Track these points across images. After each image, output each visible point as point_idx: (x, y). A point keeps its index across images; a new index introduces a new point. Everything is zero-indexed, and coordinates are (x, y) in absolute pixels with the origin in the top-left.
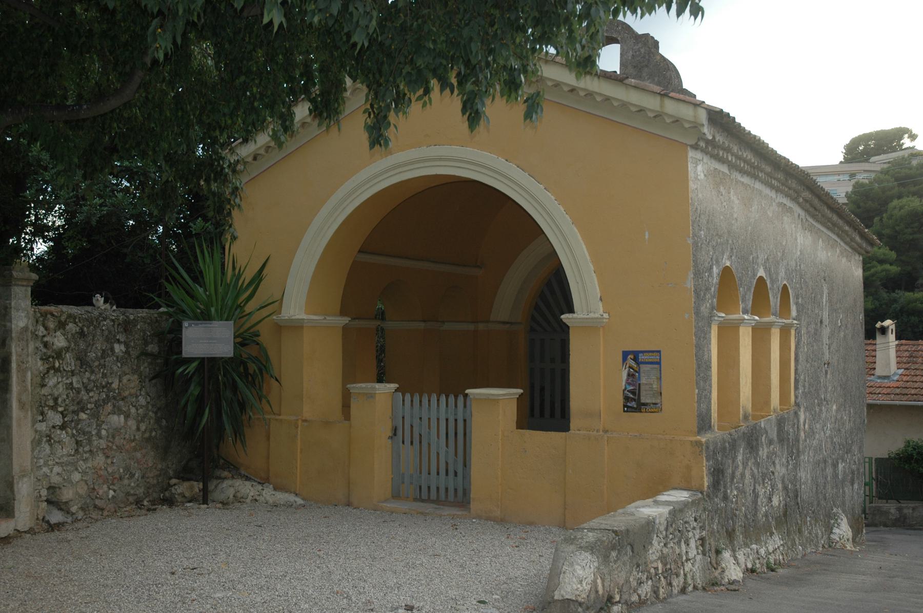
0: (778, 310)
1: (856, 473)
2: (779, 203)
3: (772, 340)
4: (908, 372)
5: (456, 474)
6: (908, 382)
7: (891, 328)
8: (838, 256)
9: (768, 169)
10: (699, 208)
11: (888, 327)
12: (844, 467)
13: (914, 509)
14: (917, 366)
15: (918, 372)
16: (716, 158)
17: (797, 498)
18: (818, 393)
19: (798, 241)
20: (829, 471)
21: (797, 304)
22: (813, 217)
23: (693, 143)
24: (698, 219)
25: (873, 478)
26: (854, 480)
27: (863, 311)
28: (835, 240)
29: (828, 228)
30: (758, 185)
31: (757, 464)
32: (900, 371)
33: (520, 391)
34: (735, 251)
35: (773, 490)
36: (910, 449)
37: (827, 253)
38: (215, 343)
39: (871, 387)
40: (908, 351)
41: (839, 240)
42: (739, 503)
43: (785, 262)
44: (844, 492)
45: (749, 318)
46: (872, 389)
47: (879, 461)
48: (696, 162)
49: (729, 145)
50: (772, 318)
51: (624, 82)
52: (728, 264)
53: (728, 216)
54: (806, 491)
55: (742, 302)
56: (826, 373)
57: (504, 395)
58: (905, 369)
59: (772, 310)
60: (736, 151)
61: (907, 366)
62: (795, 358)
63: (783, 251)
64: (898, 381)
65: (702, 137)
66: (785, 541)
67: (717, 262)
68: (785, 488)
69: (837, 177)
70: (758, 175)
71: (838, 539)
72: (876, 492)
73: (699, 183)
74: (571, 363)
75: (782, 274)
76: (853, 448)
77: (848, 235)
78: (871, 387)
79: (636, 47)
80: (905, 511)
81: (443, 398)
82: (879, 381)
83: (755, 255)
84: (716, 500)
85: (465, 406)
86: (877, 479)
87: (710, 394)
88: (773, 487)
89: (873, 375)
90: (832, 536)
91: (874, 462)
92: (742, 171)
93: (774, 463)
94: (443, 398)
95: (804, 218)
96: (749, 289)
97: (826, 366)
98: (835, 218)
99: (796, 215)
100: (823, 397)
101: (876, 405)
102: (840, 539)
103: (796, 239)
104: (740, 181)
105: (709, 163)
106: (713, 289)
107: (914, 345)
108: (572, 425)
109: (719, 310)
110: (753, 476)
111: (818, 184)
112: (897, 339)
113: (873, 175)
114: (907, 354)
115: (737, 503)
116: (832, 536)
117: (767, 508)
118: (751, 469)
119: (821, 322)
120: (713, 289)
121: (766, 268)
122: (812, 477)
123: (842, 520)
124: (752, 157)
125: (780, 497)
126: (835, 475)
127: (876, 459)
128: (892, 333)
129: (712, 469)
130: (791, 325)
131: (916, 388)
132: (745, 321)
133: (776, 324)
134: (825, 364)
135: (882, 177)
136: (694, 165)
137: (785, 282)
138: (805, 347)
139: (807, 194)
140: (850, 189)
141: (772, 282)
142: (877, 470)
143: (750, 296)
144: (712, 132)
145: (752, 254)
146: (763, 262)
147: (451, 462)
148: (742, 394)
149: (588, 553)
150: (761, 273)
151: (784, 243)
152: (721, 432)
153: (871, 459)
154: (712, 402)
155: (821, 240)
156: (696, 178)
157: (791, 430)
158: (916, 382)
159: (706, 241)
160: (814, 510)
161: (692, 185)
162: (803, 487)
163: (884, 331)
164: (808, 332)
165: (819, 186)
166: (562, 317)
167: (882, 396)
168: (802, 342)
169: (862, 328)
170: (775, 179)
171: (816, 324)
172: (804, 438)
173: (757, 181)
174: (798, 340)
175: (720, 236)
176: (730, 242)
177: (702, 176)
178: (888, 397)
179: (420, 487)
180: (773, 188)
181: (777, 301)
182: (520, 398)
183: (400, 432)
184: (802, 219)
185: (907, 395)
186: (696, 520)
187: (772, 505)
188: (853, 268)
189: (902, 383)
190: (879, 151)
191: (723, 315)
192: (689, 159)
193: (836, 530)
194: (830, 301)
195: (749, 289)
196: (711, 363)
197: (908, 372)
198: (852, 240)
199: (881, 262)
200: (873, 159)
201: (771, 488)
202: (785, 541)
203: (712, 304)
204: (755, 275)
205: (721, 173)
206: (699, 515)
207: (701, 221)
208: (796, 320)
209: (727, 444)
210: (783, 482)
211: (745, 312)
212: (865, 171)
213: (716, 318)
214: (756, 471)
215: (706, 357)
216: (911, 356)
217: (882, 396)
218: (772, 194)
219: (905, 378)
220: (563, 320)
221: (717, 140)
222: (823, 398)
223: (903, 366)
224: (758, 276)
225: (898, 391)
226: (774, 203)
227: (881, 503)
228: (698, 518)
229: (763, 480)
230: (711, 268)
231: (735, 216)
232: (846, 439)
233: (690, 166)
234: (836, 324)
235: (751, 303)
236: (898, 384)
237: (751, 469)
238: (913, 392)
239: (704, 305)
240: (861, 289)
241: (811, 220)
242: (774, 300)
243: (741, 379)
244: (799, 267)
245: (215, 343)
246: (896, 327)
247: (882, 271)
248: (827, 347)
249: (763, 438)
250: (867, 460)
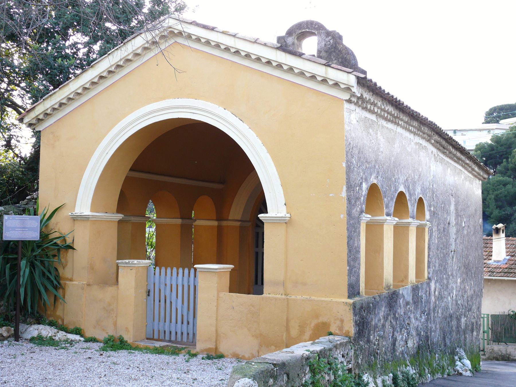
0: (415, 213)
1: (475, 324)
2: (416, 143)
3: (410, 234)
5: (188, 323)
7: (502, 229)
8: (463, 180)
9: (406, 119)
10: (352, 143)
12: (466, 321)
16: (365, 109)
17: (428, 341)
18: (446, 271)
19: (432, 169)
21: (430, 210)
22: (444, 153)
23: (347, 98)
24: (351, 150)
25: (489, 328)
26: (473, 329)
28: (460, 170)
29: (455, 161)
30: (399, 130)
31: (396, 319)
33: (232, 266)
34: (381, 173)
35: (408, 336)
37: (454, 178)
38: (27, 231)
41: (463, 170)
42: (380, 345)
43: (421, 183)
44: (465, 338)
45: (390, 219)
47: (493, 316)
48: (350, 111)
49: (374, 101)
50: (410, 220)
51: (302, 57)
52: (375, 182)
53: (376, 149)
54: (436, 337)
55: (386, 208)
56: (453, 257)
57: (220, 269)
59: (410, 214)
60: (379, 106)
62: (428, 247)
63: (420, 175)
65: (353, 95)
66: (417, 371)
67: (366, 180)
68: (419, 334)
70: (398, 123)
72: (492, 337)
73: (353, 126)
75: (418, 190)
77: (470, 167)
79: (327, 39)
81: (181, 270)
83: (396, 177)
84: (361, 343)
85: (195, 276)
86: (492, 329)
87: (359, 270)
88: (408, 333)
92: (386, 119)
93: (409, 318)
94: (181, 270)
95: (436, 154)
96: (392, 199)
97: (453, 253)
98: (459, 154)
99: (430, 152)
100: (450, 273)
103: (430, 167)
104: (386, 127)
105: (361, 113)
106: (362, 198)
108: (266, 288)
109: (367, 213)
110: (392, 326)
111: (443, 131)
115: (378, 344)
117: (403, 348)
118: (391, 322)
119: (449, 224)
120: (362, 198)
121: (406, 186)
122: (441, 328)
124: (392, 110)
125: (414, 341)
126: (458, 326)
127: (492, 315)
128: (503, 233)
129: (358, 322)
130: (426, 225)
132: (387, 221)
133: (412, 223)
134: (451, 252)
136: (349, 114)
137: (421, 196)
138: (436, 240)
139: (436, 137)
141: (410, 195)
142: (492, 322)
143: (392, 204)
144: (360, 91)
145: (394, 176)
146: (403, 182)
147: (185, 314)
148: (385, 271)
149: (251, 379)
150: (402, 189)
151: (420, 170)
152: (367, 296)
154: (361, 275)
155: (449, 169)
156: (350, 123)
157: (424, 295)
159: (357, 165)
160: (442, 349)
161: (347, 128)
162: (433, 334)
164: (439, 230)
165: (444, 132)
166: (259, 216)
167: (496, 274)
168: (434, 237)
170: (412, 126)
171: (445, 225)
172: (434, 301)
173: (399, 127)
174: (431, 234)
175: (369, 163)
176: (377, 167)
177: (354, 122)
179: (165, 331)
181: (414, 209)
182: (232, 271)
183: (152, 294)
184: (434, 155)
186: (343, 356)
187: (407, 347)
188: (475, 188)
191: (370, 216)
192: (345, 110)
194: (456, 210)
195: (392, 199)
196: (360, 249)
198: (473, 170)
200: (502, 122)
201: (407, 334)
202: (417, 371)
203: (361, 209)
204: (396, 190)
205: (370, 121)
206: (346, 353)
207: (353, 151)
208: (429, 222)
209: (371, 305)
210: (417, 330)
211: (388, 215)
213: (364, 218)
214: (394, 323)
215: (356, 245)
217: (496, 274)
218: (412, 136)
220: (260, 218)
221: (364, 97)
222: (450, 274)
224: (399, 191)
225: (506, 270)
226: (412, 143)
228: (345, 355)
229: (401, 329)
230: (361, 183)
231: (381, 150)
232: (468, 301)
233: (346, 114)
234: (461, 225)
235: (393, 209)
237: (391, 322)
239: (355, 209)
240: (481, 202)
241: (442, 155)
242: (412, 208)
243: (384, 261)
244: (432, 187)
245: (27, 231)
248: (454, 240)
249: (401, 301)
250: (486, 316)
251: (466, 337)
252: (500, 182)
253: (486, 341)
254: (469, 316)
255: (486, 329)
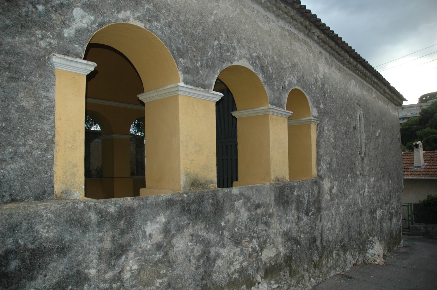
4: (429, 165)
6: (429, 168)
11: (419, 144)
13: (433, 228)
14: (434, 162)
15: (434, 164)
20: (366, 217)
25: (412, 213)
27: (399, 132)
32: (426, 164)
36: (429, 200)
39: (412, 171)
40: (429, 155)
46: (412, 172)
58: (428, 163)
61: (429, 161)
64: (424, 168)
69: (416, 108)
71: (370, 257)
74: (216, 156)
76: (392, 201)
78: (412, 171)
80: (429, 229)
82: (415, 169)
86: (415, 213)
89: (413, 166)
90: (367, 255)
91: (413, 206)
101: (413, 179)
102: (372, 256)
107: (433, 153)
112: (424, 150)
113: (428, 106)
114: (429, 156)
116: (367, 255)
123: (376, 244)
127: (414, 204)
131: (433, 171)
135: (431, 106)
140: (420, 111)
153: (411, 204)
158: (433, 168)
163: (417, 146)
169: (399, 141)
178: (418, 176)
180: (301, 31)
185: (429, 174)
189: (426, 169)
190: (430, 99)
193: (370, 251)
197: (429, 165)
199: (432, 134)
212: (426, 105)
216: (431, 157)
219: (428, 167)
223: (427, 162)
225: (424, 173)
227: (417, 225)
236: (424, 170)
238: (431, 173)
246: (423, 145)
247: (433, 137)
250: (409, 205)
251: (383, 225)
252: (323, 104)
253: (410, 222)
254: (386, 208)
255: (410, 214)
